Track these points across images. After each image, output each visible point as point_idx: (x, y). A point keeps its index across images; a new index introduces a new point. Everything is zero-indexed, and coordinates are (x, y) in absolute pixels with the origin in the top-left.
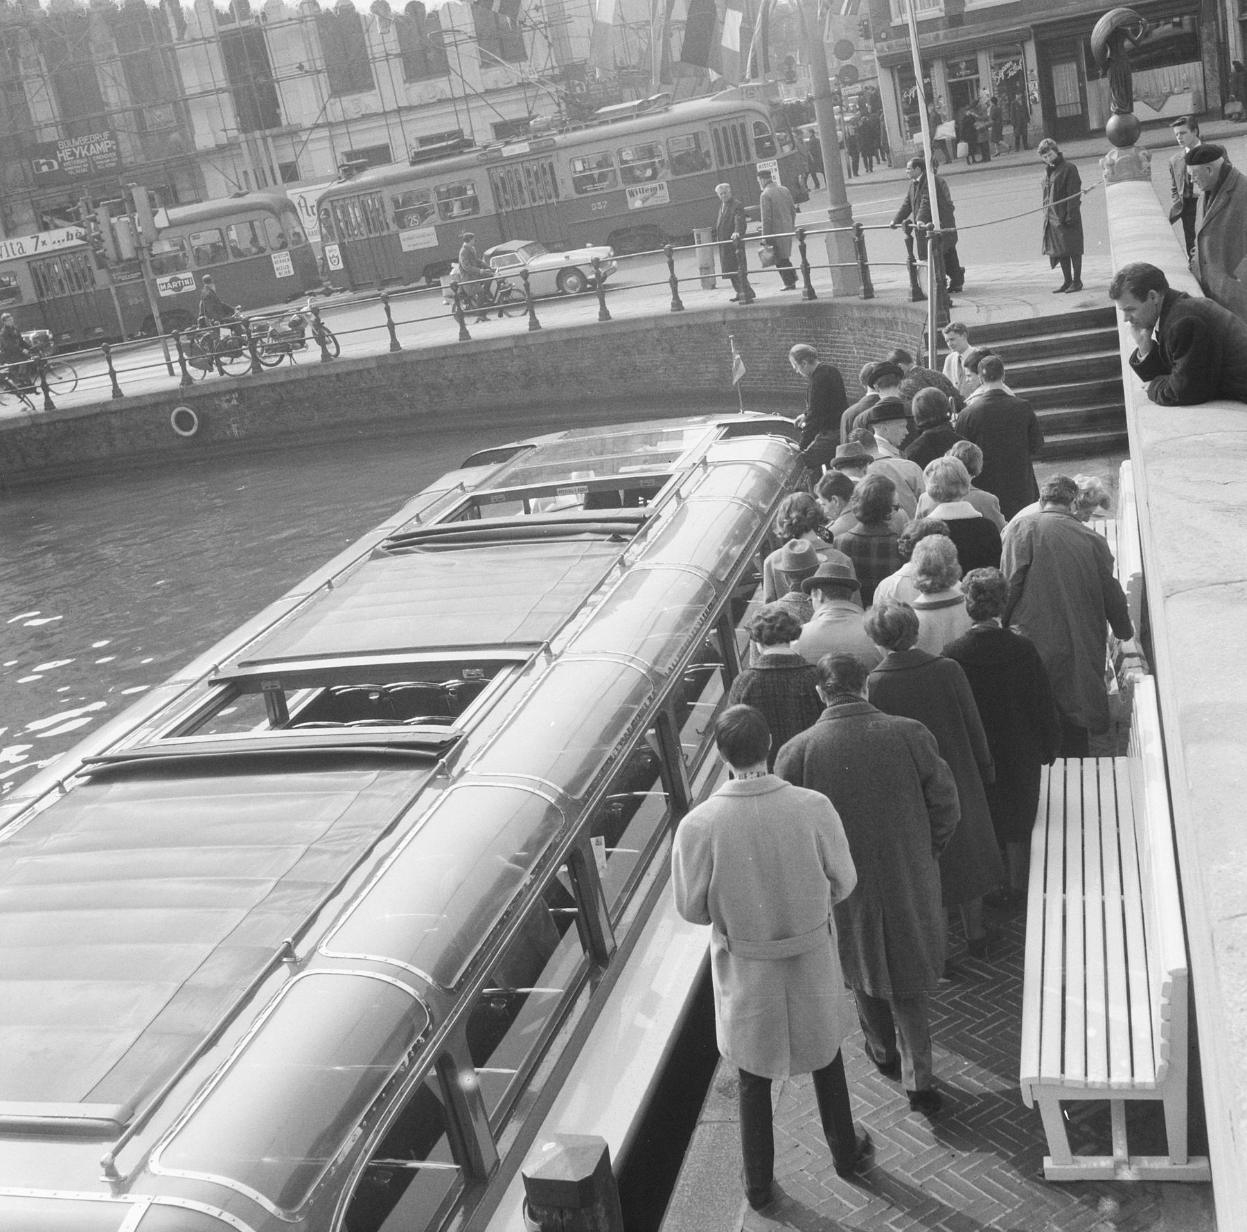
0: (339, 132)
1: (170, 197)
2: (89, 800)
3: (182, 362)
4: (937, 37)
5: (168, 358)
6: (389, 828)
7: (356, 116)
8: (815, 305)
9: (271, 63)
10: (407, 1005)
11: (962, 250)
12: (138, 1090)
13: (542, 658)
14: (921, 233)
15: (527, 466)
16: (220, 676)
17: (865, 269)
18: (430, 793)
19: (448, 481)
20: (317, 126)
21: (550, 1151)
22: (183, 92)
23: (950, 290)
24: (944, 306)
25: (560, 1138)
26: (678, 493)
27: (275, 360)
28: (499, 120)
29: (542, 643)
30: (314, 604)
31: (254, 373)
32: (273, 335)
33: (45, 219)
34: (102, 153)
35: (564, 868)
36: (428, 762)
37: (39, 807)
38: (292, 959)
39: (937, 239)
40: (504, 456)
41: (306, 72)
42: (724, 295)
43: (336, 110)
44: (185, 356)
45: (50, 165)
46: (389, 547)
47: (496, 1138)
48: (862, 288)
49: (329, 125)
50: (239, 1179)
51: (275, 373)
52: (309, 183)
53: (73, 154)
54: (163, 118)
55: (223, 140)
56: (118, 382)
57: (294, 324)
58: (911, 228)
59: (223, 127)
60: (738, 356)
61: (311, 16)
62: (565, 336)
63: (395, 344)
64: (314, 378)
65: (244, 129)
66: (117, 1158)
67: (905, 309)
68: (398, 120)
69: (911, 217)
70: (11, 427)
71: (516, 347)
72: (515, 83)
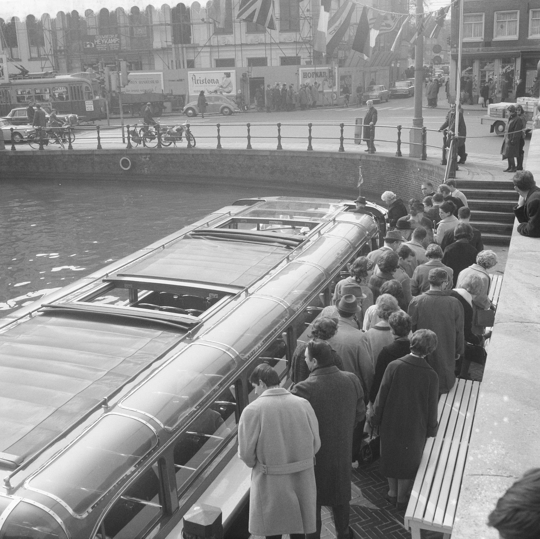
1: (139, 67)
2: (40, 323)
3: (129, 138)
5: (123, 136)
6: (160, 357)
7: (223, 44)
8: (400, 159)
9: (191, 17)
11: (468, 144)
12: (28, 451)
13: (243, 295)
14: (450, 136)
15: (260, 209)
17: (424, 148)
18: (182, 344)
19: (225, 210)
22: (152, 22)
23: (459, 163)
24: (454, 168)
25: (203, 506)
26: (319, 232)
27: (167, 144)
28: (283, 55)
29: (245, 288)
30: (155, 254)
31: (158, 148)
33: (85, 67)
34: (113, 43)
35: (233, 386)
36: (183, 331)
37: (19, 321)
38: (106, 406)
39: (456, 140)
40: (251, 203)
41: (205, 22)
42: (363, 148)
43: (215, 41)
44: (131, 136)
45: (91, 45)
46: (192, 235)
47: (179, 498)
48: (422, 155)
49: (211, 46)
51: (167, 149)
52: (198, 70)
53: (101, 42)
54: (141, 32)
55: (165, 45)
56: (101, 142)
58: (447, 133)
62: (292, 154)
63: (219, 146)
65: (175, 42)
66: (11, 479)
67: (438, 168)
68: (234, 49)
69: (447, 128)
72: (293, 41)
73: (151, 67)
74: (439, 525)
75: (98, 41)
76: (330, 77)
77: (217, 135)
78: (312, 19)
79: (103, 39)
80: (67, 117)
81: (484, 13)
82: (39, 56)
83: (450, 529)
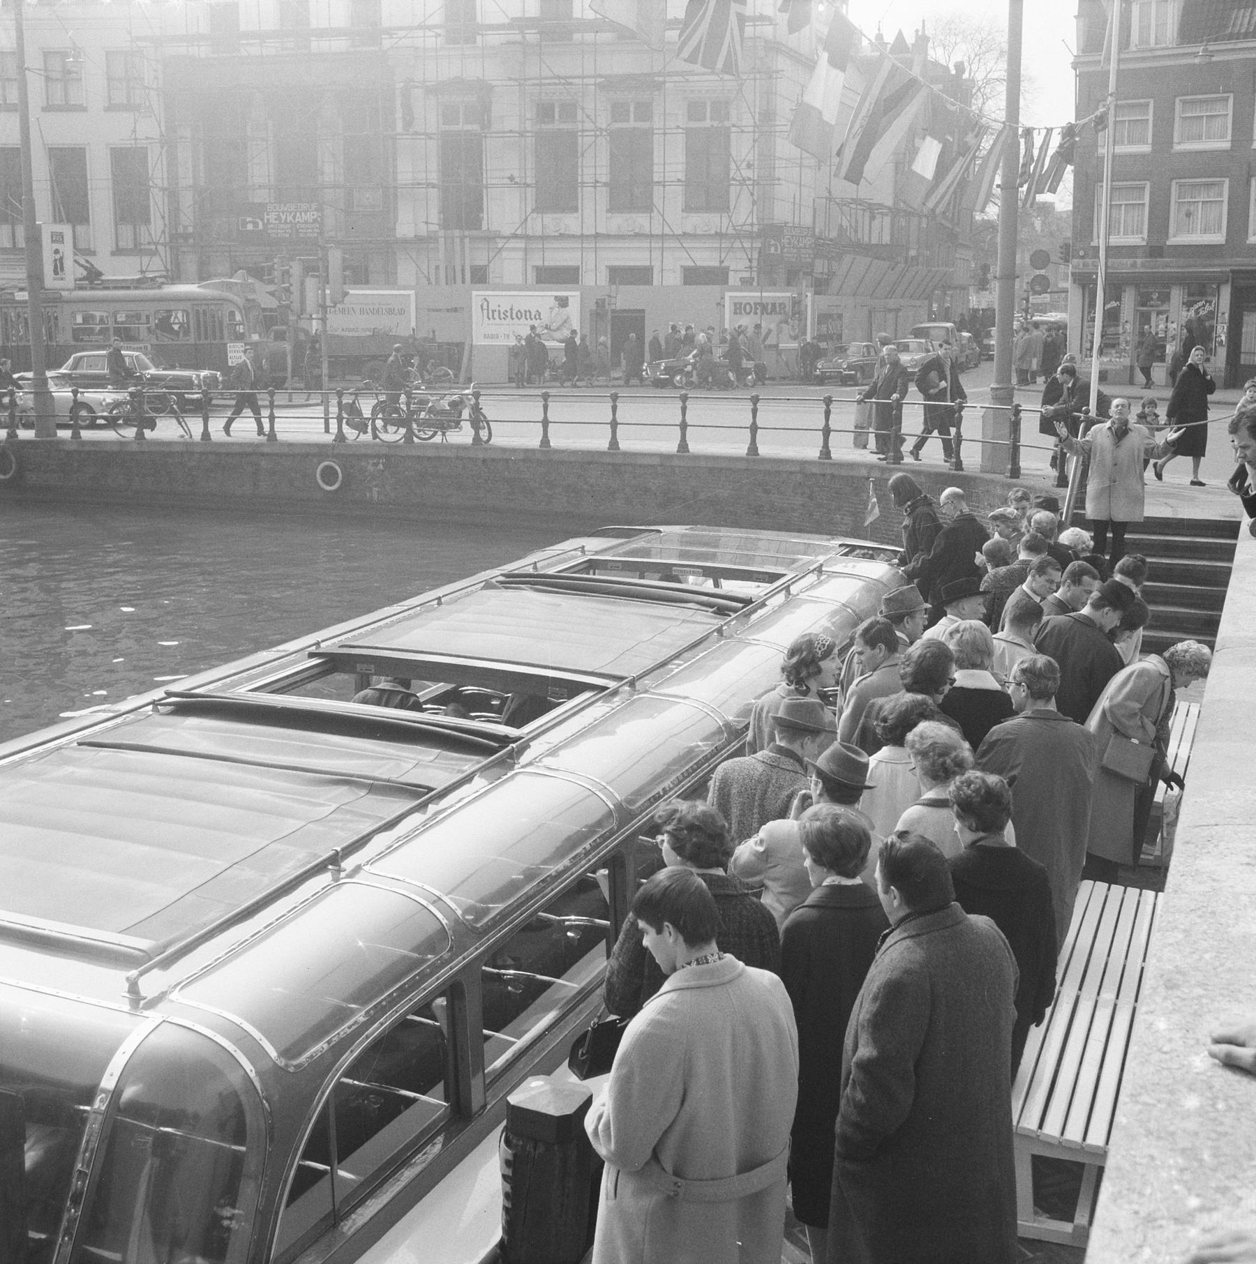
0: (533, 246)
4: (1134, 265)
5: (327, 412)
8: (960, 476)
10: (431, 928)
16: (320, 651)
17: (1015, 450)
20: (515, 236)
21: (537, 1087)
22: (395, 179)
26: (787, 589)
28: (690, 264)
32: (430, 411)
34: (306, 222)
38: (337, 868)
40: (628, 534)
41: (516, 183)
42: (868, 456)
44: (345, 415)
45: (255, 224)
46: (501, 583)
48: (1009, 467)
49: (527, 237)
50: (248, 1021)
51: (423, 446)
52: (496, 287)
53: (279, 218)
55: (423, 231)
57: (453, 404)
59: (425, 220)
60: (875, 500)
61: (532, 132)
63: (545, 441)
64: (462, 459)
65: (445, 225)
70: (166, 449)
71: (661, 465)
72: (713, 232)
73: (390, 279)
74: (1075, 1142)
75: (272, 217)
76: (794, 315)
77: (541, 418)
78: (758, 184)
79: (283, 212)
80: (198, 376)
81: (1148, 184)
82: (135, 245)
83: (1102, 1154)
